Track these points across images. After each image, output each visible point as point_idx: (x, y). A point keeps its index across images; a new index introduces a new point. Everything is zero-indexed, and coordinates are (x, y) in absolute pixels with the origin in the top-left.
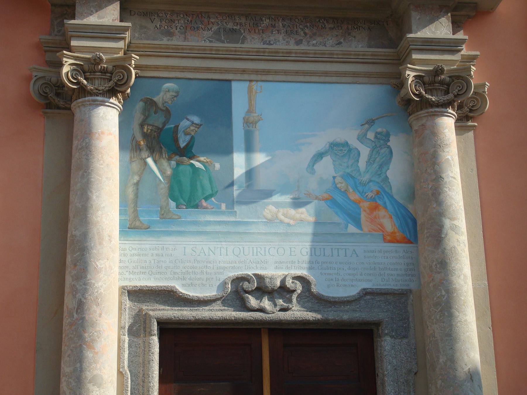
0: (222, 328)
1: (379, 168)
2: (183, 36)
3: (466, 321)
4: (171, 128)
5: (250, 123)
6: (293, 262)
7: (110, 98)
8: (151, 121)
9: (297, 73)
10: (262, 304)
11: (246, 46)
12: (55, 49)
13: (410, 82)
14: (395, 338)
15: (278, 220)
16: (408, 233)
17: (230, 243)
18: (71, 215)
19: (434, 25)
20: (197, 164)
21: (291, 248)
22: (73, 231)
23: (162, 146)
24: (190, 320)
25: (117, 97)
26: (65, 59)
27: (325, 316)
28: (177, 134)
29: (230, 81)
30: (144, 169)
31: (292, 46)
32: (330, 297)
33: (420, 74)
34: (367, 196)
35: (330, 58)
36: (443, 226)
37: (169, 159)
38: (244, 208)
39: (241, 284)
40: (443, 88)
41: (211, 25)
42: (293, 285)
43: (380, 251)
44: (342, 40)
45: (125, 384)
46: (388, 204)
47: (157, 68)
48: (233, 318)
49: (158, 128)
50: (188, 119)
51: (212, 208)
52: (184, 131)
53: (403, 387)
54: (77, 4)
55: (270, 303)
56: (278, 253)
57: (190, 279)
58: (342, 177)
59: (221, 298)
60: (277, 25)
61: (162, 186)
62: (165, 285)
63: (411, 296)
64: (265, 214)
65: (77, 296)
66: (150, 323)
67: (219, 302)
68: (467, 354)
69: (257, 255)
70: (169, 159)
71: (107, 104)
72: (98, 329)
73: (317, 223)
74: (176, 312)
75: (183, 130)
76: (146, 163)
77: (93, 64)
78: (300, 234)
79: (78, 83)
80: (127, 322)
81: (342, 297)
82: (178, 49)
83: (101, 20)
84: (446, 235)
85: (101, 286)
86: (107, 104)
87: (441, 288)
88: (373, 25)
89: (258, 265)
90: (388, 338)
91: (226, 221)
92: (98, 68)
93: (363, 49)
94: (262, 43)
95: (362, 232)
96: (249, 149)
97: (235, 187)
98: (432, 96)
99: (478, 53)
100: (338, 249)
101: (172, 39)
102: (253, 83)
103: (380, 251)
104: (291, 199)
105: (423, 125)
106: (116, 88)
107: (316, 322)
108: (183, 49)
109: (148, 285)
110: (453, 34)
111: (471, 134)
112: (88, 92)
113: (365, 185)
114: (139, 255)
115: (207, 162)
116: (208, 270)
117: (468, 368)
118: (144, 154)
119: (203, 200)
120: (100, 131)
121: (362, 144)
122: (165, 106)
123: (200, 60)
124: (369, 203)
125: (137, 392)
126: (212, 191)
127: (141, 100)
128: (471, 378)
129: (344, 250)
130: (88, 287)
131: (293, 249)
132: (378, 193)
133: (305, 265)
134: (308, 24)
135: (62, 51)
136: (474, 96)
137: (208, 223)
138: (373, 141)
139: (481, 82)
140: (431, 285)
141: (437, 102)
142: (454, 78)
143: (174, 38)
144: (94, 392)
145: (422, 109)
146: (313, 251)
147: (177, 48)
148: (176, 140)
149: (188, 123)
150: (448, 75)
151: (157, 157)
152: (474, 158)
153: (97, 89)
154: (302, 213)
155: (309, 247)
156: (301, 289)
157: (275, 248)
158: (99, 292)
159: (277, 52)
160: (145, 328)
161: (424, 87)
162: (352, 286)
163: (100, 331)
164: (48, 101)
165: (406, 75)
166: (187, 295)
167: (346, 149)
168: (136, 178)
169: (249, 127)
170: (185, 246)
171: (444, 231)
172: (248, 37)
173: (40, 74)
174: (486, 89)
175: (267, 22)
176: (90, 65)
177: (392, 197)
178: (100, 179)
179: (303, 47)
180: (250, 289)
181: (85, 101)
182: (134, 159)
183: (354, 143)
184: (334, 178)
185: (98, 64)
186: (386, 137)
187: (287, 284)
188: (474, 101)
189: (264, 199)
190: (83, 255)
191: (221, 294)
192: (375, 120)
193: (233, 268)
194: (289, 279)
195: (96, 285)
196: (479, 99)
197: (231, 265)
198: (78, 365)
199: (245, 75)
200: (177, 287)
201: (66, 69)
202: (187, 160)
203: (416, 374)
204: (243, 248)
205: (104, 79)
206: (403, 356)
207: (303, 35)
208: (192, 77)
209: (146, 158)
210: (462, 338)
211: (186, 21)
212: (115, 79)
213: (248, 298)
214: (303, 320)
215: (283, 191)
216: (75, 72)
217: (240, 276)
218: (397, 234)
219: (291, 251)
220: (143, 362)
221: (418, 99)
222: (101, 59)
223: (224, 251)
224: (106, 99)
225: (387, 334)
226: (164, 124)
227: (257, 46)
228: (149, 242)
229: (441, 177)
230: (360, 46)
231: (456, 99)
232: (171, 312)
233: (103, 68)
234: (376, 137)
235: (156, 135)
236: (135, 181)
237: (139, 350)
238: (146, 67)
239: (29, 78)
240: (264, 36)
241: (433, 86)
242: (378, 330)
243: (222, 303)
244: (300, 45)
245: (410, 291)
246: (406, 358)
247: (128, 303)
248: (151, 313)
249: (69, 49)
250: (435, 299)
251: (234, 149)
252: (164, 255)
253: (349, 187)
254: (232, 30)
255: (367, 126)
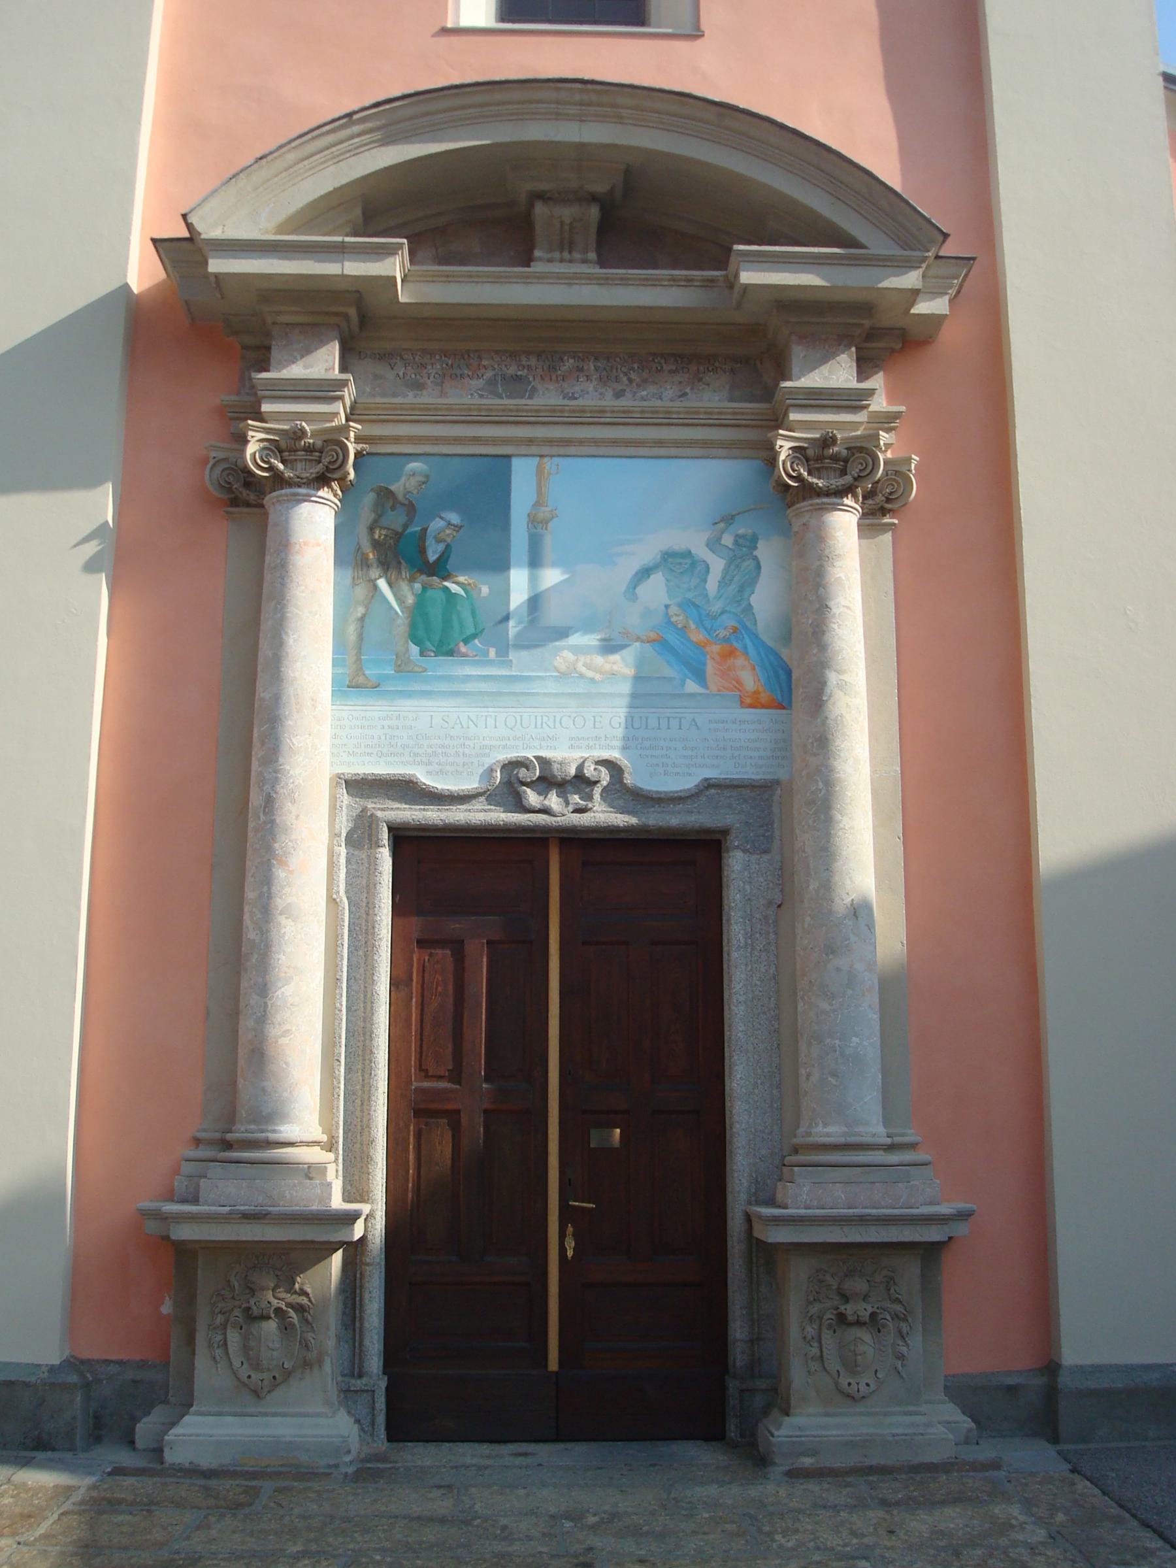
0: (475, 837)
1: (739, 591)
2: (440, 388)
3: (852, 828)
4: (416, 532)
5: (538, 523)
6: (597, 738)
7: (318, 489)
8: (384, 522)
9: (615, 442)
10: (546, 802)
11: (537, 401)
12: (242, 415)
13: (782, 457)
14: (750, 853)
15: (577, 673)
16: (779, 692)
17: (501, 710)
18: (259, 668)
19: (828, 365)
20: (454, 588)
21: (594, 717)
22: (263, 693)
23: (402, 561)
24: (437, 825)
25: (330, 487)
26: (250, 433)
27: (643, 819)
28: (424, 541)
29: (509, 457)
30: (373, 596)
31: (609, 401)
32: (652, 791)
33: (801, 444)
34: (717, 635)
35: (667, 419)
36: (825, 683)
37: (412, 580)
38: (524, 654)
39: (515, 772)
40: (838, 466)
41: (483, 370)
42: (595, 774)
43: (734, 722)
44: (688, 390)
45: (340, 917)
46: (749, 645)
47: (398, 440)
48: (502, 823)
49: (397, 533)
50: (441, 518)
51: (476, 656)
52: (435, 537)
53: (759, 926)
54: (273, 347)
55: (561, 800)
56: (574, 724)
57: (439, 764)
58: (680, 605)
59: (485, 792)
60: (585, 368)
61: (399, 622)
62: (400, 772)
63: (779, 789)
64: (556, 664)
65: (265, 788)
66: (377, 828)
67: (482, 799)
68: (850, 878)
69: (542, 727)
70: (412, 580)
71: (314, 499)
72: (293, 837)
73: (638, 679)
74: (416, 813)
75: (433, 534)
76: (376, 587)
77: (293, 439)
78: (611, 695)
79: (271, 468)
80: (344, 825)
81: (671, 792)
82: (429, 410)
83: (308, 371)
84: (830, 696)
85: (299, 774)
86: (314, 499)
87: (818, 779)
88: (739, 365)
89: (544, 744)
90: (739, 854)
91: (496, 676)
92: (300, 444)
93: (722, 405)
94: (561, 397)
95: (708, 692)
96: (535, 562)
97: (511, 623)
98: (819, 478)
99: (903, 408)
100: (669, 718)
101: (421, 395)
102: (546, 459)
103: (734, 722)
104: (600, 640)
105: (804, 524)
106: (329, 475)
107: (628, 829)
108: (436, 409)
109: (367, 772)
110: (858, 381)
111: (888, 537)
112: (286, 481)
113: (715, 618)
114: (363, 727)
115: (470, 584)
116: (467, 751)
117: (850, 899)
118: (374, 572)
119: (462, 644)
120: (301, 540)
121: (713, 552)
122: (406, 499)
123: (465, 425)
124: (718, 647)
125: (358, 929)
126: (476, 629)
127: (372, 490)
128: (855, 914)
129: (678, 720)
130: (280, 776)
131: (598, 719)
132: (735, 630)
133: (618, 744)
134: (636, 366)
135: (246, 419)
136: (894, 477)
137: (468, 678)
138: (731, 549)
139: (900, 454)
140: (804, 773)
141: (826, 489)
142: (855, 451)
143: (425, 392)
144: (288, 928)
145: (804, 499)
146: (630, 721)
147: (426, 408)
148: (422, 551)
149: (442, 524)
150: (845, 446)
151: (393, 577)
152: (891, 576)
153: (298, 477)
154: (614, 663)
155: (623, 716)
156: (608, 779)
157: (570, 717)
158: (295, 784)
159: (583, 411)
160: (370, 835)
161: (808, 465)
162: (690, 774)
163: (297, 840)
164: (233, 496)
165: (777, 447)
166: (433, 787)
167: (689, 561)
168: (361, 610)
169: (536, 528)
170: (432, 713)
171: (828, 690)
172: (539, 387)
173: (221, 455)
174: (913, 466)
175: (570, 363)
176: (288, 441)
177: (757, 637)
178: (301, 613)
179: (625, 402)
180: (529, 780)
181: (281, 496)
182: (359, 582)
183: (701, 551)
184: (667, 607)
185: (301, 438)
186: (753, 541)
187: (586, 771)
188: (893, 485)
189: (556, 640)
190: (273, 728)
191: (484, 786)
192: (735, 515)
193: (505, 747)
194: (590, 764)
195: (291, 772)
196: (900, 481)
197: (502, 743)
198: (265, 889)
199: (533, 447)
200: (419, 776)
201: (252, 448)
202: (439, 581)
203: (779, 906)
204: (521, 716)
205: (311, 461)
206: (762, 880)
207: (627, 382)
208: (450, 453)
209: (376, 579)
210: (844, 853)
211: (444, 365)
212: (325, 461)
213: (525, 792)
214: (609, 826)
215: (587, 627)
216: (266, 452)
217: (514, 759)
218: (762, 695)
219: (595, 722)
220: (368, 886)
221: (796, 485)
222: (303, 431)
223: (491, 721)
224: (313, 492)
225: (737, 847)
226: (405, 527)
227: (552, 402)
228: (379, 708)
229: (827, 606)
230: (717, 398)
231: (856, 483)
232: (409, 813)
233: (307, 445)
234: (736, 542)
235: (392, 544)
236: (359, 615)
237: (361, 868)
238: (380, 439)
239: (205, 461)
240: (565, 385)
241: (821, 463)
242: (726, 840)
243: (487, 800)
244: (622, 398)
245: (777, 782)
246: (766, 883)
247: (345, 799)
248: (379, 814)
249: (259, 417)
250: (808, 794)
251: (512, 564)
252: (400, 727)
253: (691, 622)
254: (515, 377)
255: (722, 525)
